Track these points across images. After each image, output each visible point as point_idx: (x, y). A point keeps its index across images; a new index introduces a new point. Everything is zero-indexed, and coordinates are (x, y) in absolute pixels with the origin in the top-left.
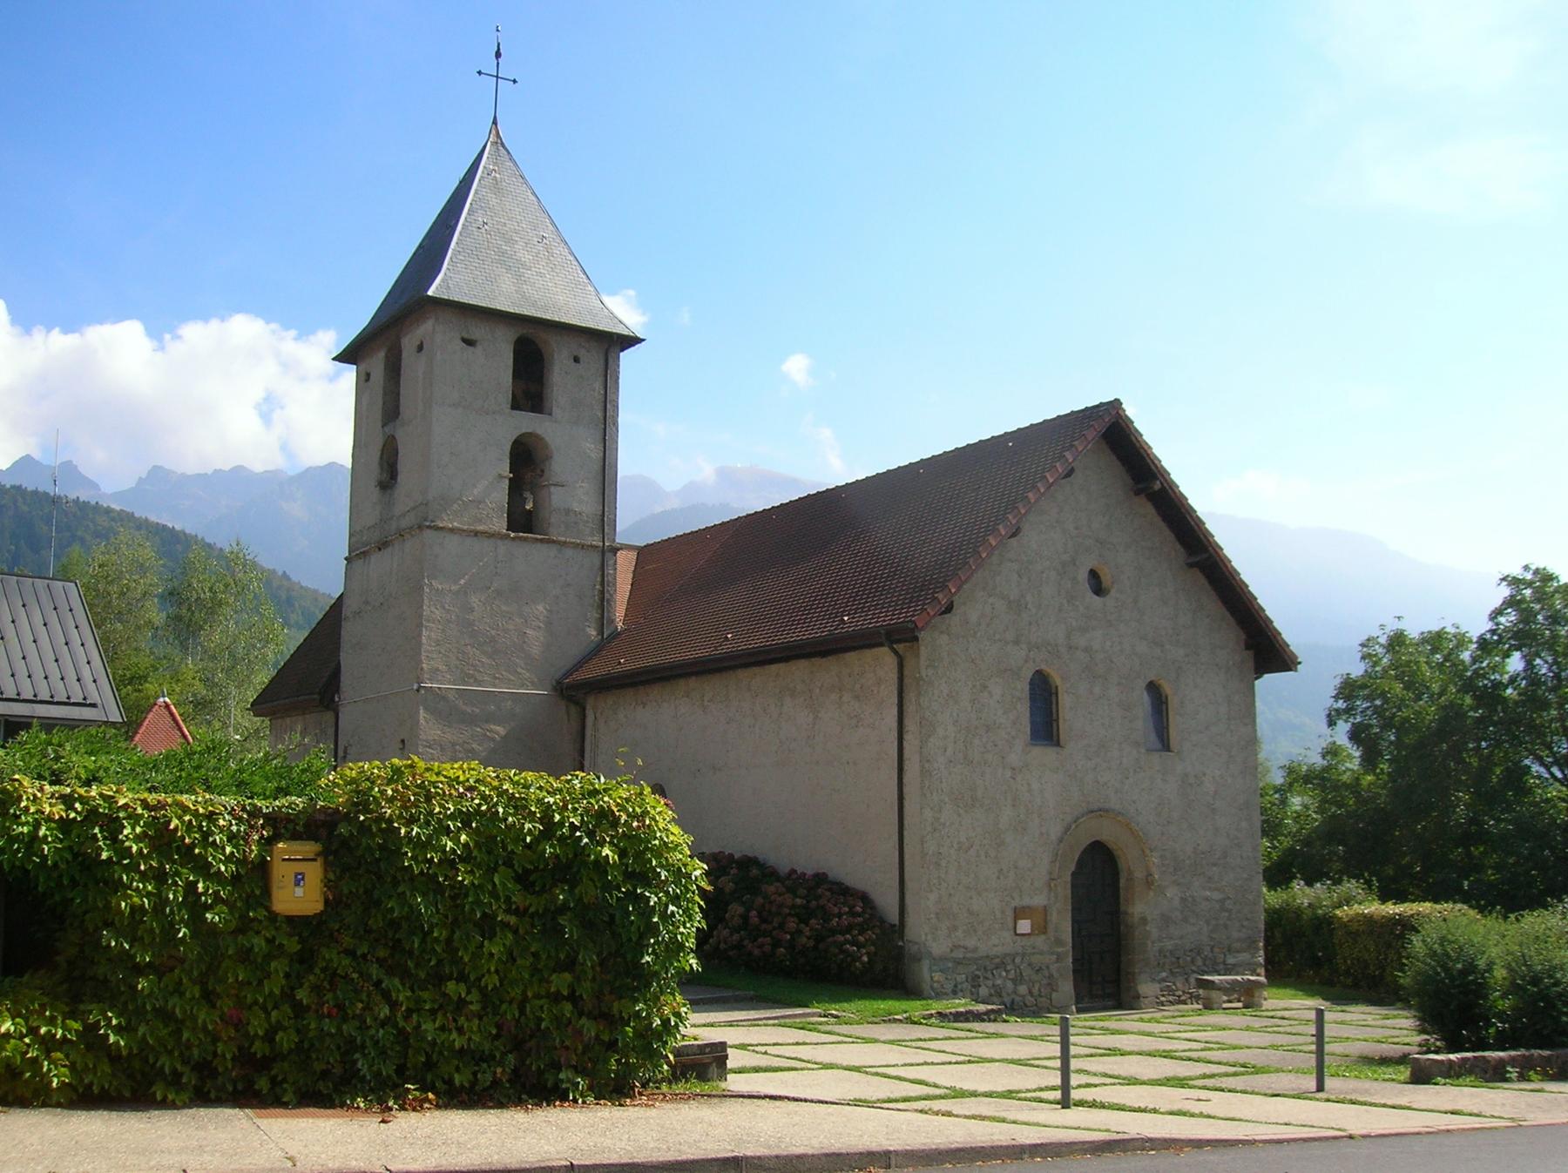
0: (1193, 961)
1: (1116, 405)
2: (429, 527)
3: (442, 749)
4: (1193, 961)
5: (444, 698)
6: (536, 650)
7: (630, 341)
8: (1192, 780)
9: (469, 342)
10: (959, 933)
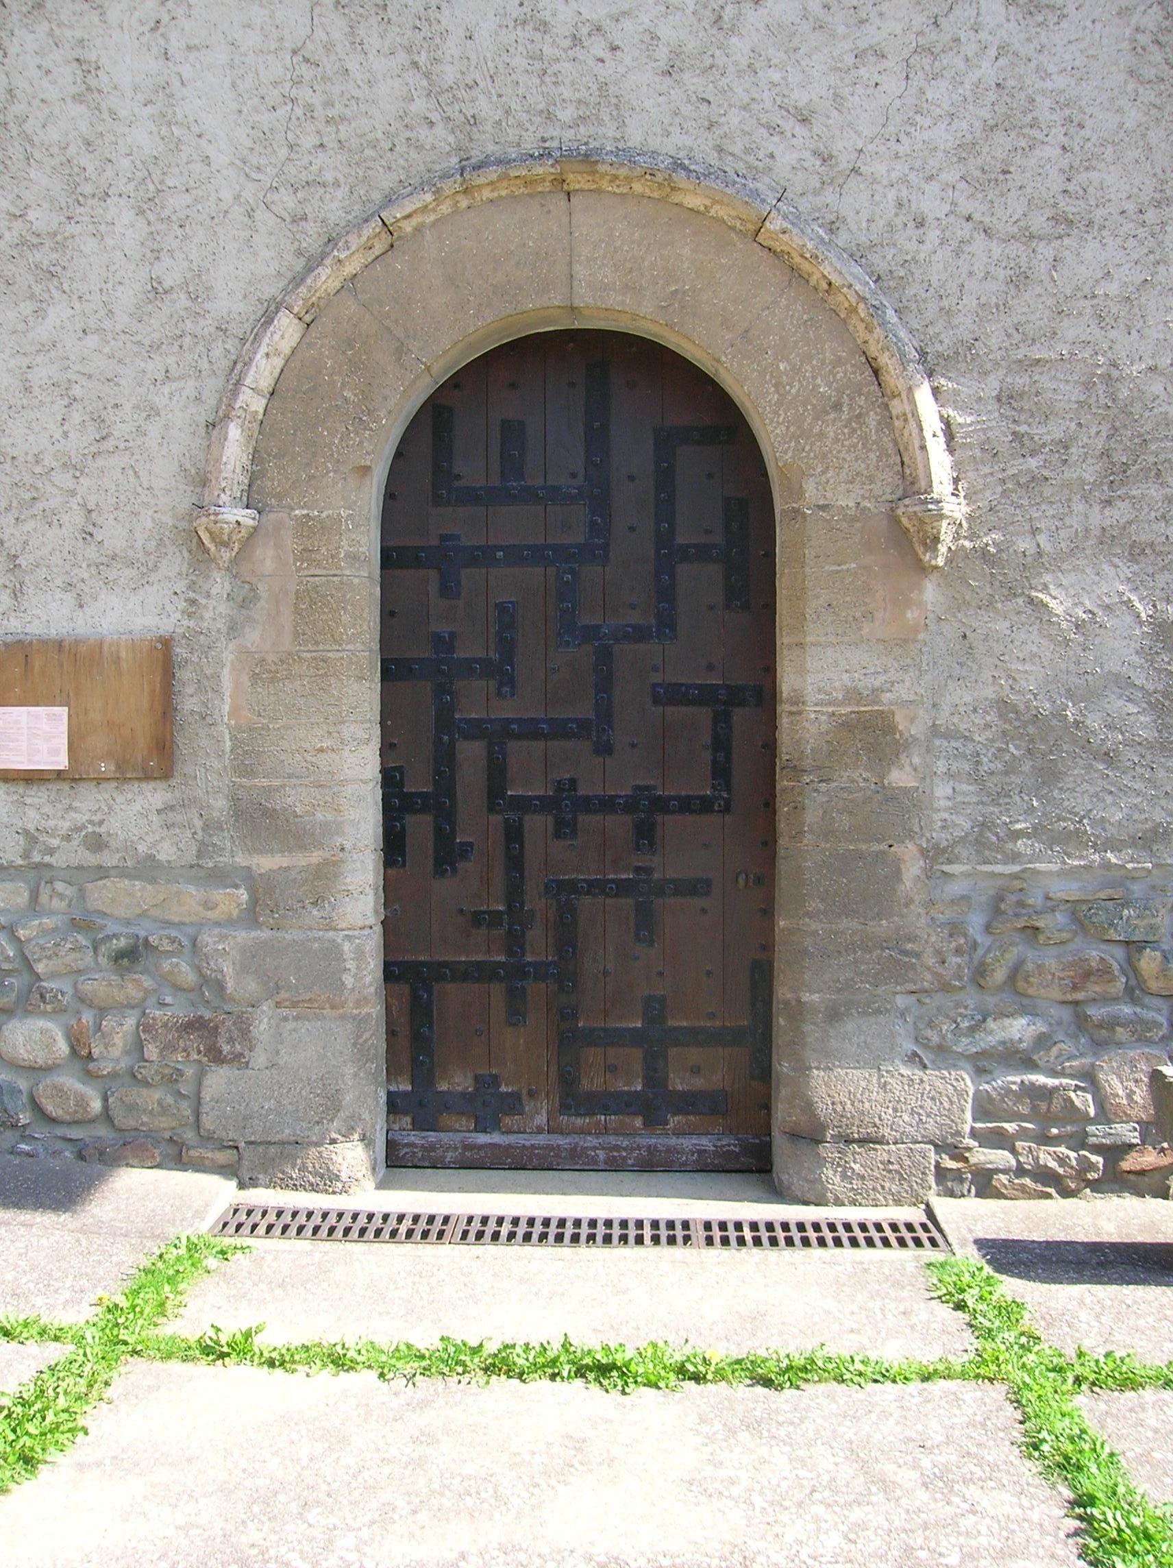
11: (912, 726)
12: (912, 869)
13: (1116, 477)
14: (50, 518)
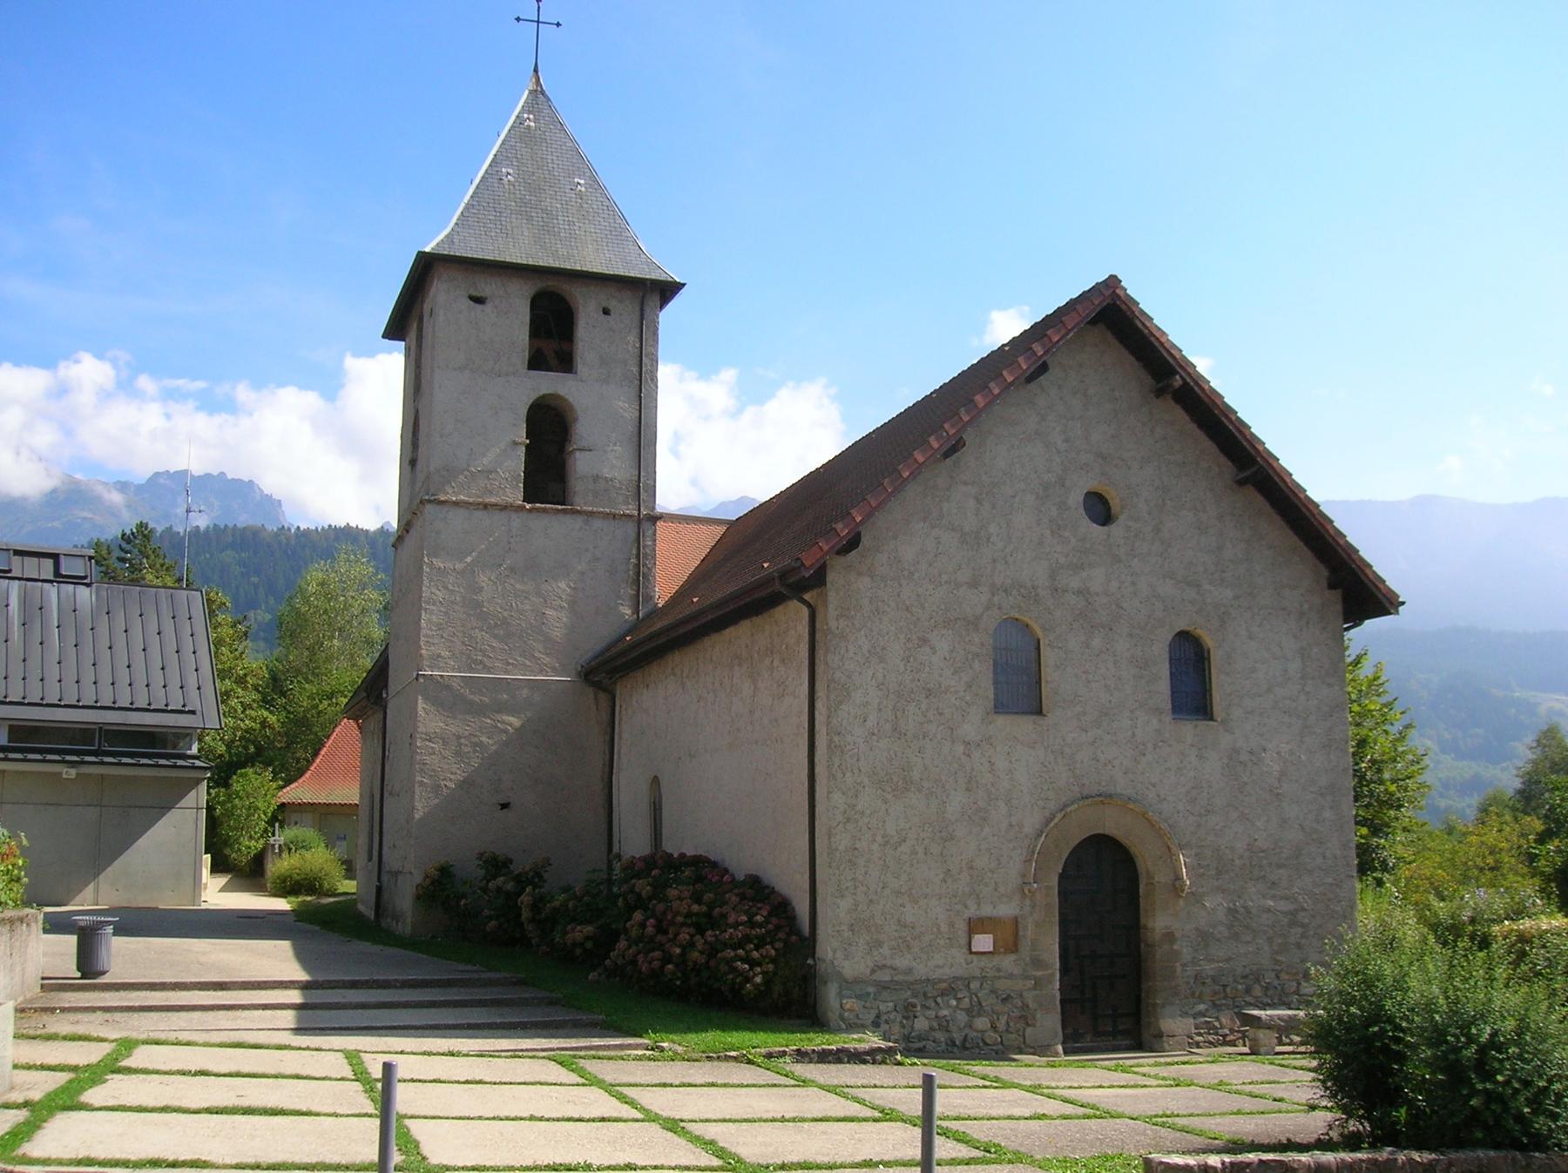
0: (1248, 991)
1: (1113, 282)
2: (429, 501)
3: (445, 743)
4: (1248, 991)
5: (448, 687)
6: (557, 633)
7: (667, 290)
8: (1244, 757)
9: (479, 300)
10: (885, 950)
11: (1178, 935)
12: (1179, 969)
13: (1219, 873)
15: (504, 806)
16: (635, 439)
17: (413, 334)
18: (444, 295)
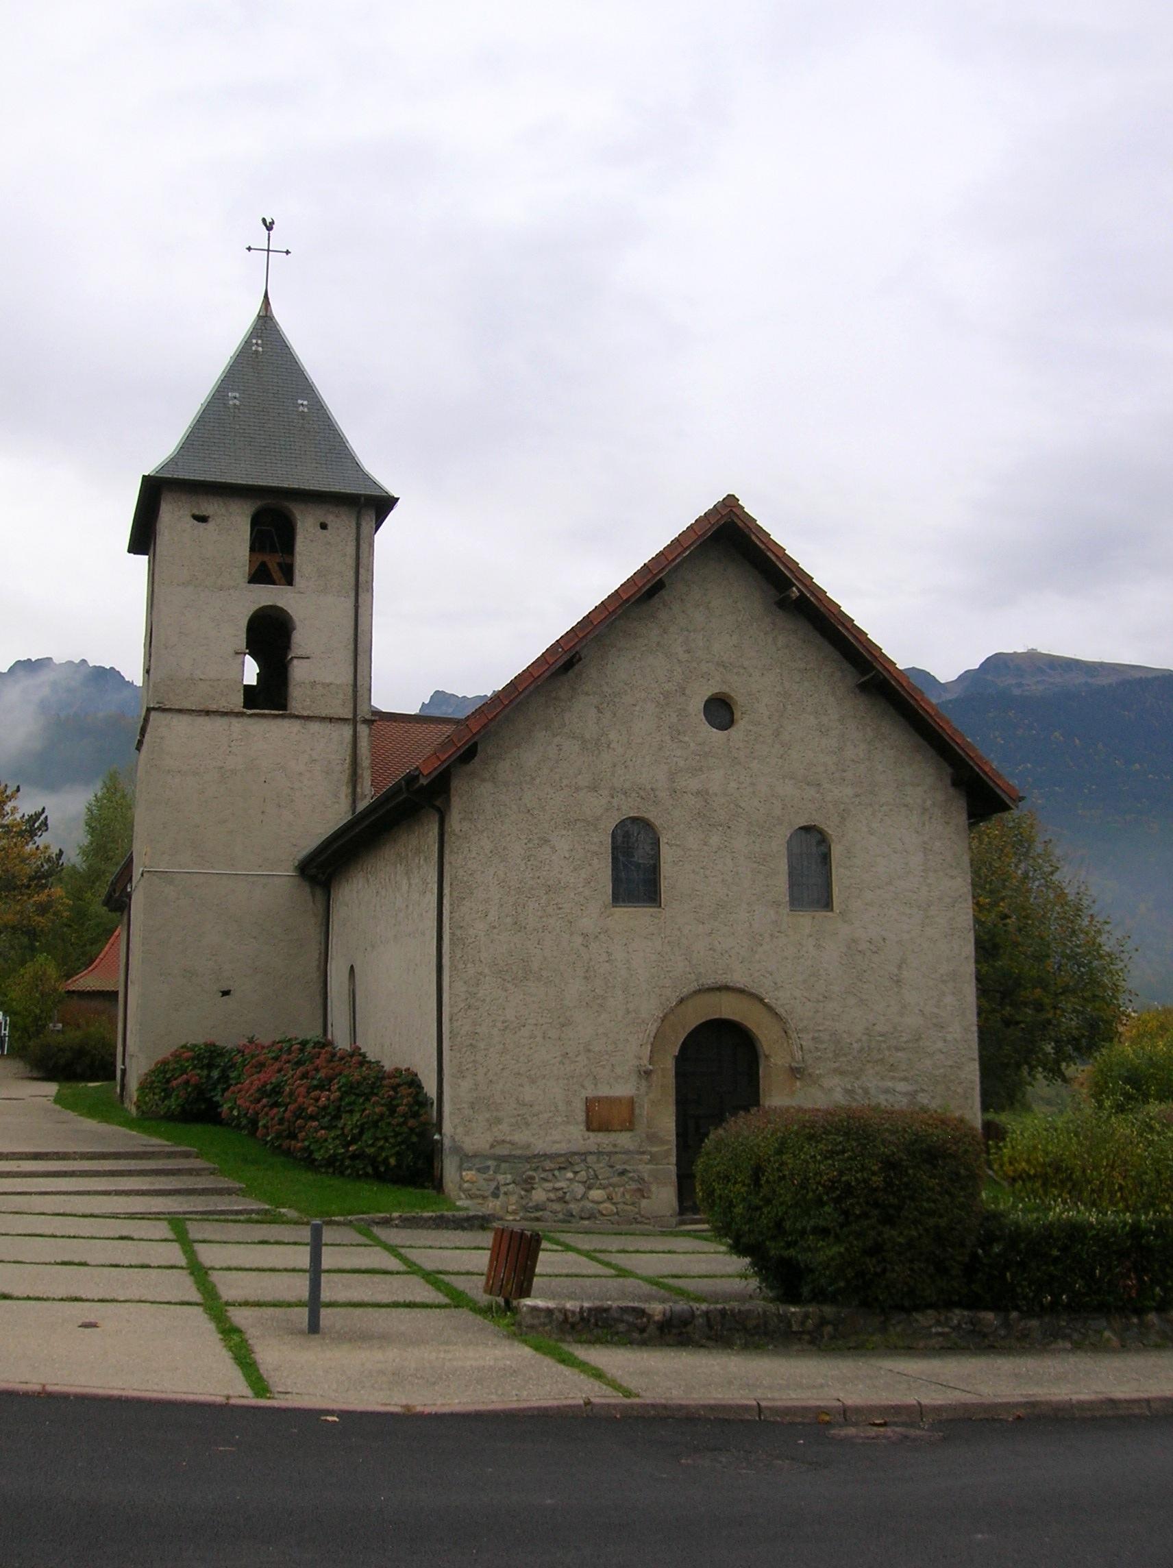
1: (730, 505)
8: (863, 946)
9: (202, 519)
10: (504, 1127)
14: (603, 1067)
15: (226, 993)
16: (351, 647)
17: (151, 551)
18: (172, 516)
